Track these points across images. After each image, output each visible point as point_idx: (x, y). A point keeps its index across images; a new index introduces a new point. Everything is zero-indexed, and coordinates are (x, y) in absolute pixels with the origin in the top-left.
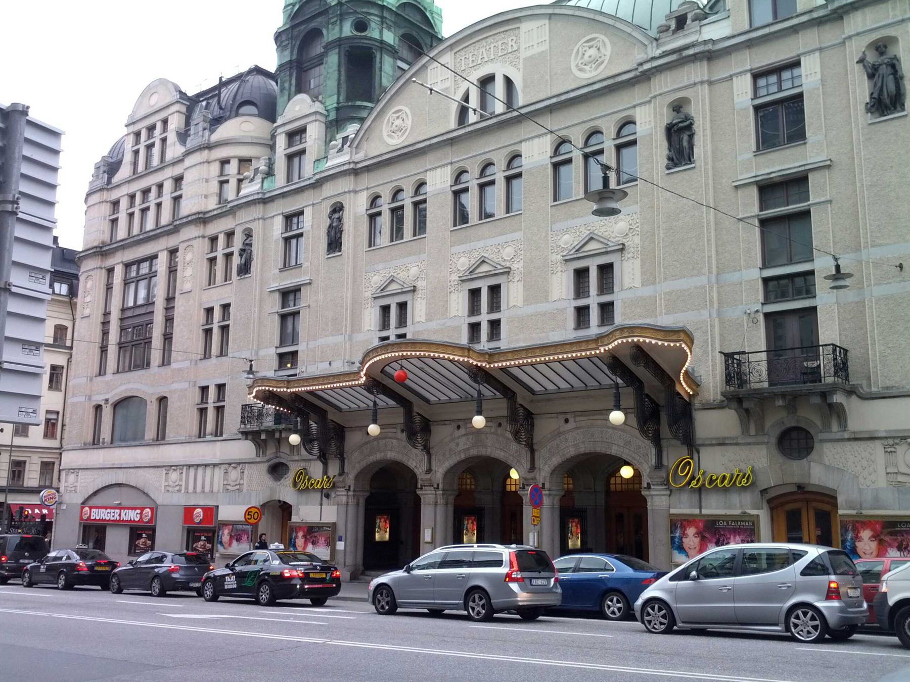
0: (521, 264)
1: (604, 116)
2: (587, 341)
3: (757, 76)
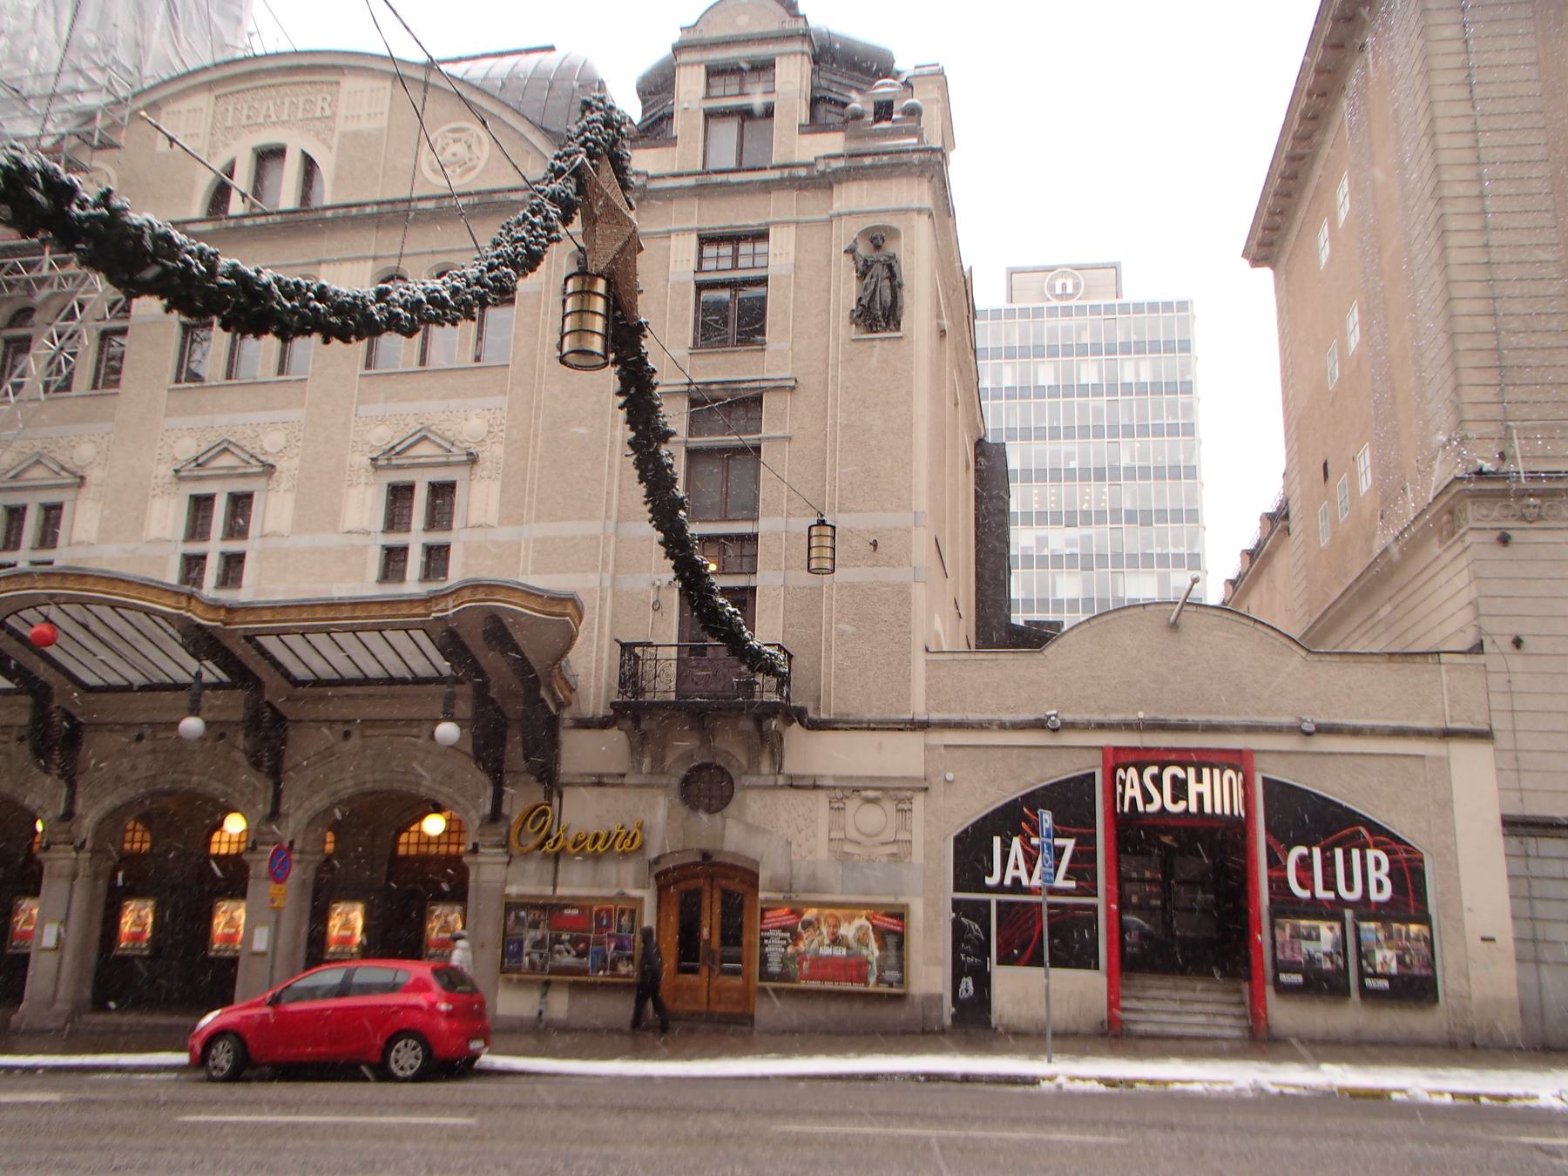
0: (296, 462)
2: (412, 602)
3: (705, 240)
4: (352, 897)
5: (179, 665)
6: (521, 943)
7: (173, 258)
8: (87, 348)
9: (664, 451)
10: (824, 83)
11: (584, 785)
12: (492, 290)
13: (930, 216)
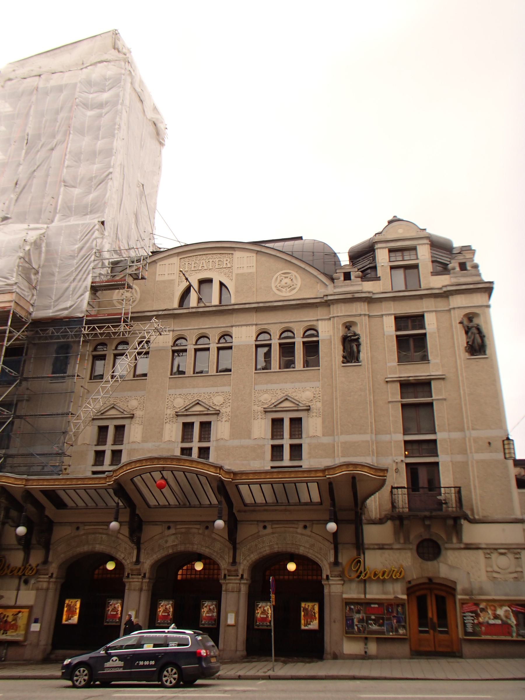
0: (229, 409)
1: (298, 322)
6: (353, 620)
11: (374, 549)
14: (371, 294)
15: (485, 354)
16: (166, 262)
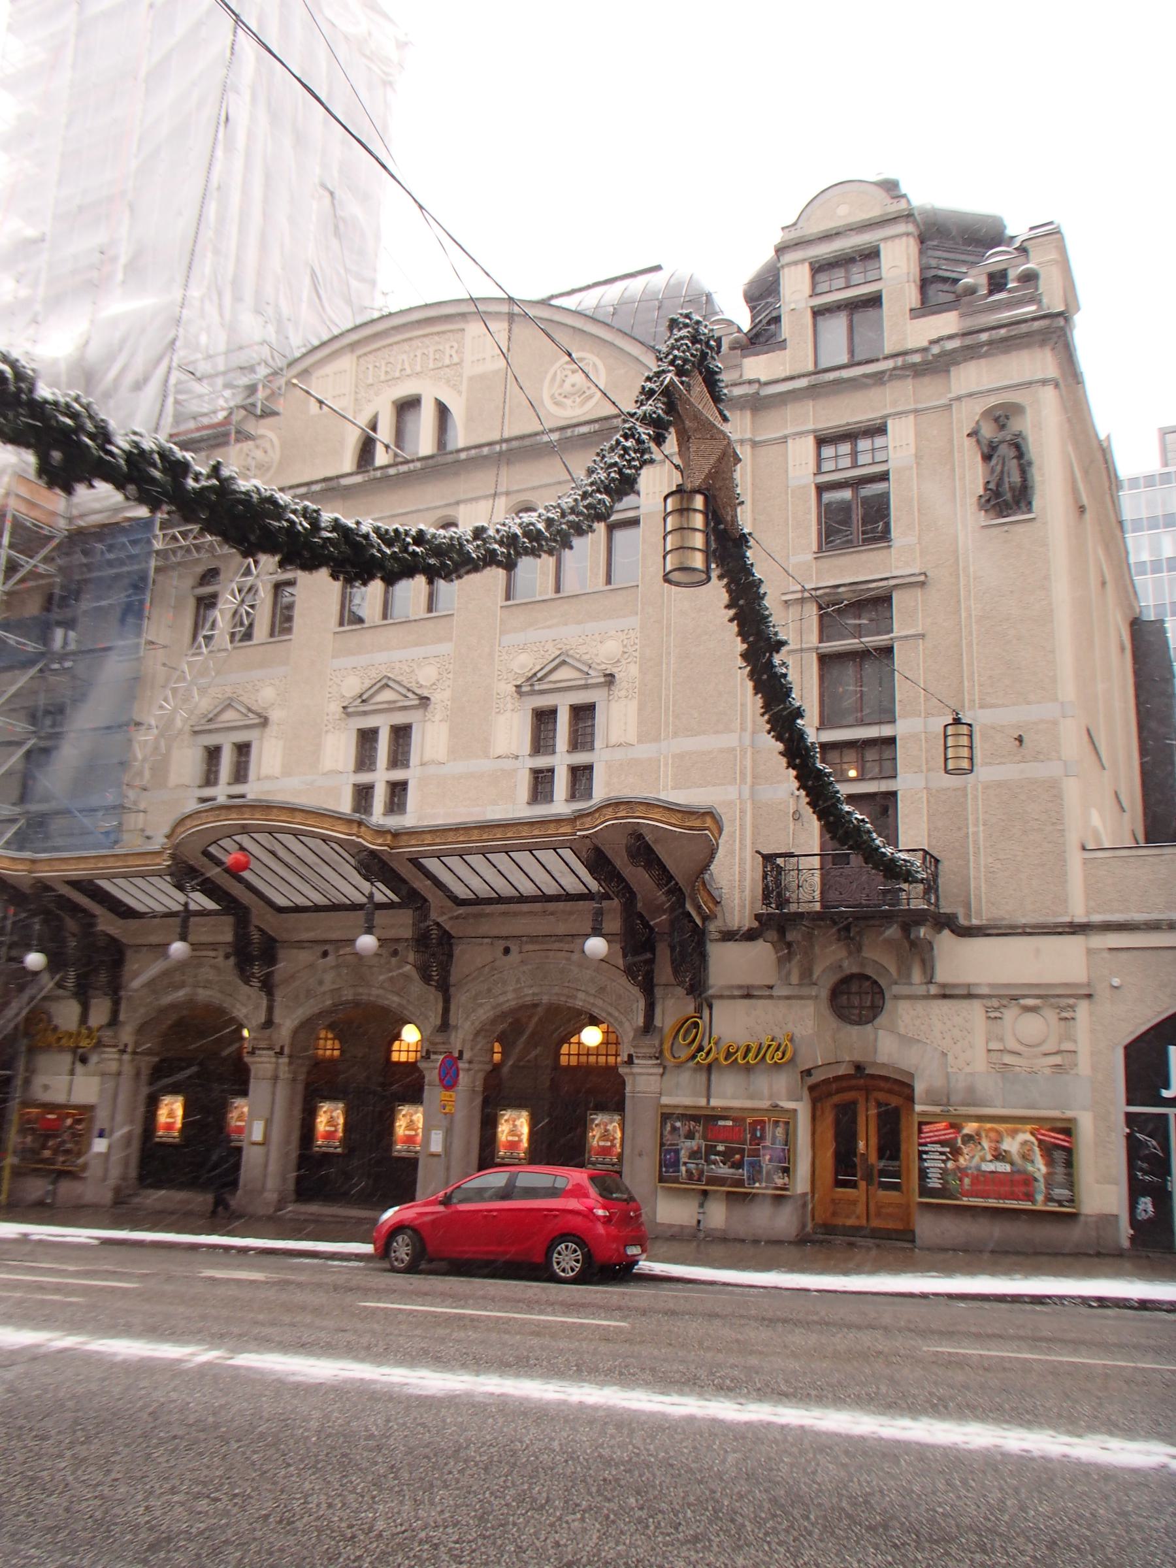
0: (447, 694)
4: (519, 1106)
5: (353, 887)
6: (677, 1152)
7: (279, 518)
8: (263, 601)
9: (777, 659)
10: (933, 263)
11: (733, 997)
12: (587, 517)
13: (1057, 386)
14: (756, 386)
15: (1030, 511)
16: (329, 369)
